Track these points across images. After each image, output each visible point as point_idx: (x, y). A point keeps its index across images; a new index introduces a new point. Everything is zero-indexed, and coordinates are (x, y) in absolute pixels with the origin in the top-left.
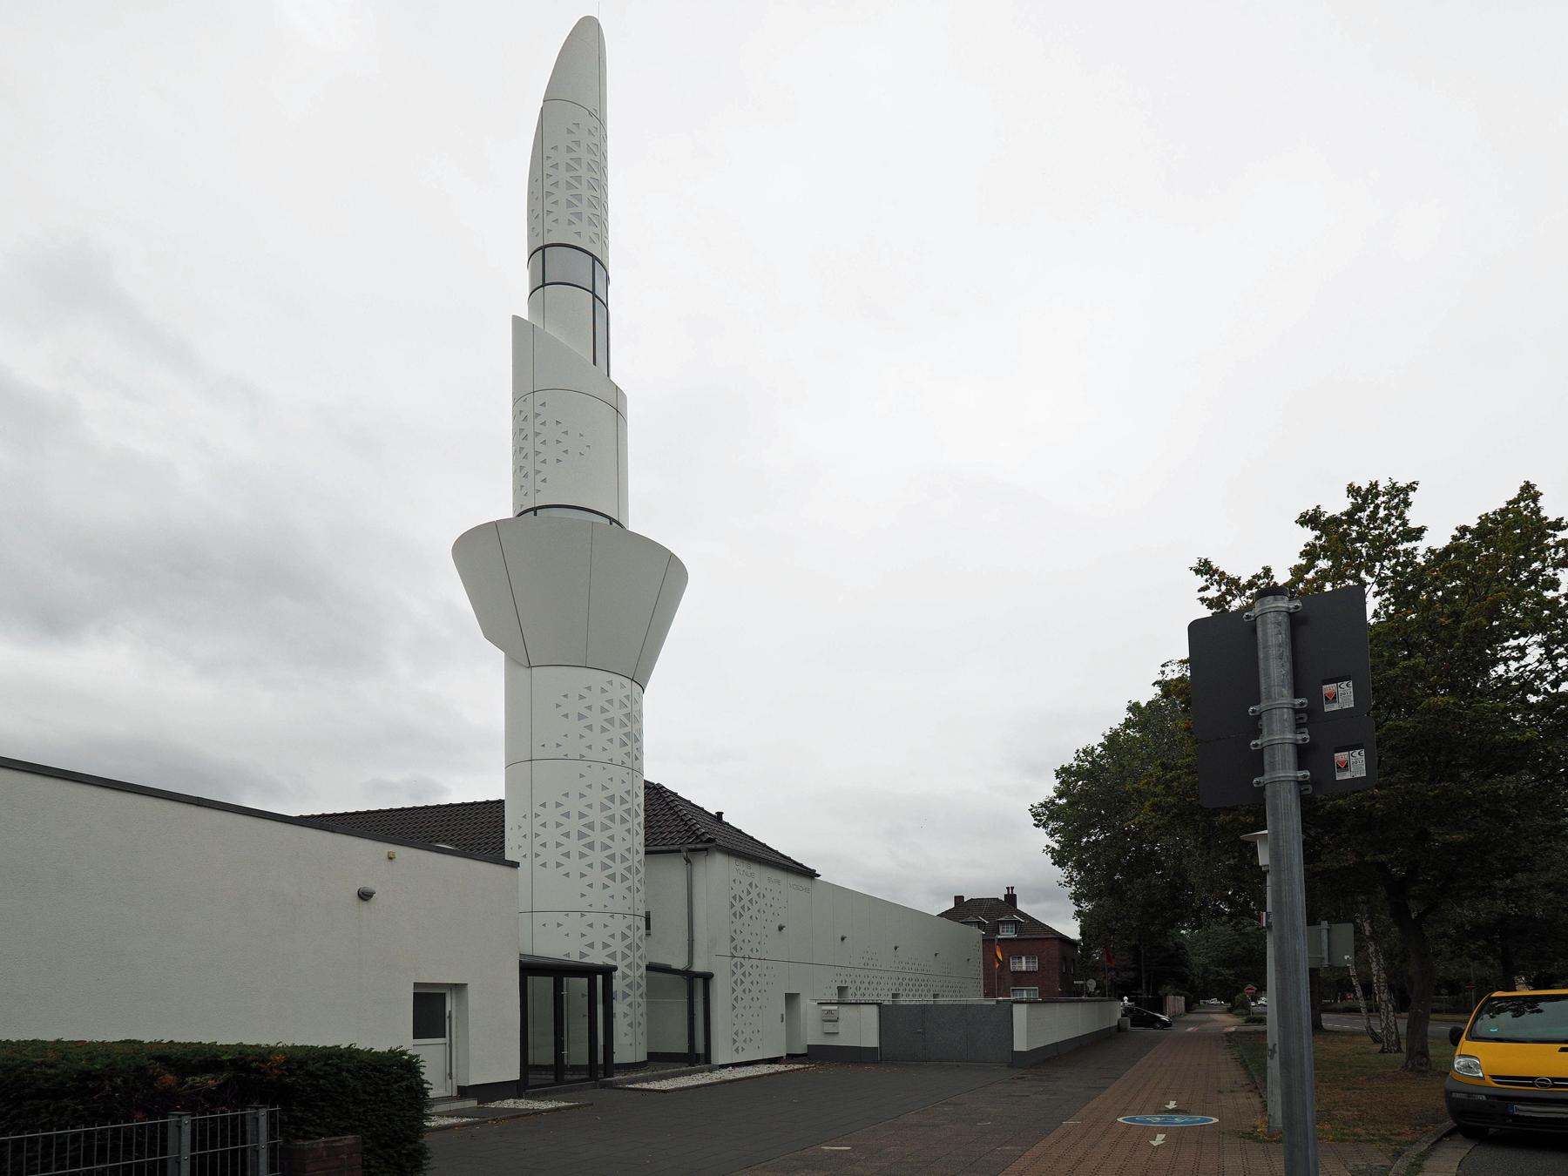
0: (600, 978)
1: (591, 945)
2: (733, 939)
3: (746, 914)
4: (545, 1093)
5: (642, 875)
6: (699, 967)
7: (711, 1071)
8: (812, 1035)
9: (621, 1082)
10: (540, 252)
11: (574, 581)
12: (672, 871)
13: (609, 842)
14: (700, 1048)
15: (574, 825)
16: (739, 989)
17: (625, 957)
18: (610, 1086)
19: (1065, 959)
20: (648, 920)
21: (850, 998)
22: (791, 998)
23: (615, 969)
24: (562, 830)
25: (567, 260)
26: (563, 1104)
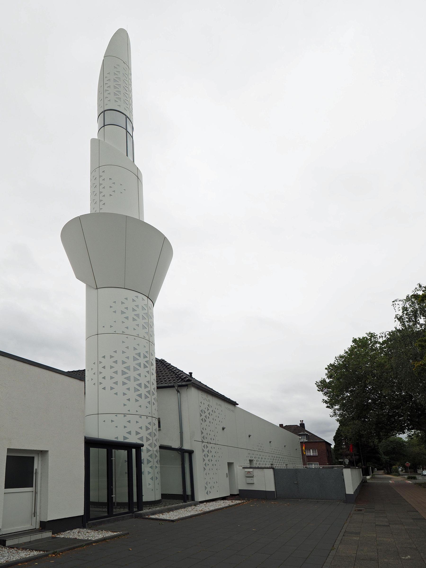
0: (134, 451)
1: (130, 433)
2: (202, 433)
3: (208, 420)
4: (101, 523)
5: (155, 396)
6: (186, 447)
7: (195, 505)
8: (241, 484)
9: (148, 514)
10: (103, 113)
11: (118, 250)
12: (170, 396)
13: (138, 377)
14: (189, 492)
15: (120, 367)
16: (207, 459)
17: (148, 439)
18: (141, 516)
19: (328, 450)
20: (159, 423)
21: (254, 465)
22: (230, 465)
23: (143, 445)
24: (113, 370)
25: (115, 115)
26: (110, 534)
